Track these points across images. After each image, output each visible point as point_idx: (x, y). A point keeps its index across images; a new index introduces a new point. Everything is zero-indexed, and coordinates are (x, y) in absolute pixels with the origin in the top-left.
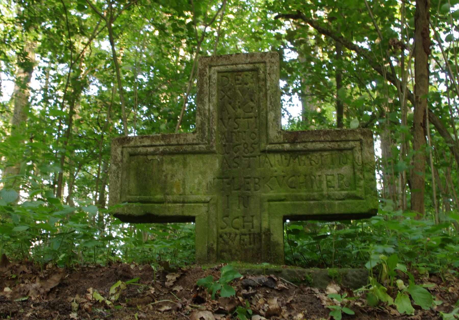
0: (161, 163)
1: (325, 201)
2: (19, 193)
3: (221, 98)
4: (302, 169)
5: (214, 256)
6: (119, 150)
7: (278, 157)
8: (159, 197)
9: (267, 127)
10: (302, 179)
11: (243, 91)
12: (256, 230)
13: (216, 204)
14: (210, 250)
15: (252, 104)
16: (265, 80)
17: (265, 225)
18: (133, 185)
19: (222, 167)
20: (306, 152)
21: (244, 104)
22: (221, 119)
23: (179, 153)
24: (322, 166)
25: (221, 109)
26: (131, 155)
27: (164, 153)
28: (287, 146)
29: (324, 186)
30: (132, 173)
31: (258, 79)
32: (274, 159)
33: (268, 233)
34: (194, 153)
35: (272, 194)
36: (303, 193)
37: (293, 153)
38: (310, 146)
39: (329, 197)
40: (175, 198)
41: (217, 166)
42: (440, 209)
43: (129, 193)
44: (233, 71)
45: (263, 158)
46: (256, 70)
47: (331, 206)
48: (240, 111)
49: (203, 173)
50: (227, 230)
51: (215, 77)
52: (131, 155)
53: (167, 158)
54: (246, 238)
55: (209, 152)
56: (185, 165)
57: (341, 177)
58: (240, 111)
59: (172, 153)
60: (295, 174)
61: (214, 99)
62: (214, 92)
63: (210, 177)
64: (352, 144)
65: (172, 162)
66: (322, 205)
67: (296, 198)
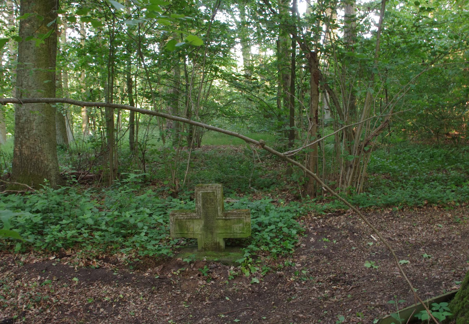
0: (186, 222)
1: (235, 234)
2: (205, 6)
3: (203, 201)
4: (228, 224)
5: (203, 249)
6: (172, 218)
7: (221, 220)
8: (186, 232)
9: (217, 212)
10: (228, 227)
11: (210, 199)
12: (215, 242)
13: (203, 235)
14: (202, 248)
15: (213, 203)
16: (217, 196)
17: (218, 241)
18: (178, 228)
19: (204, 223)
20: (230, 219)
21: (210, 203)
22: (203, 208)
23: (191, 219)
24: (234, 223)
25: (203, 205)
26: (176, 219)
27: (186, 219)
28: (224, 218)
29: (235, 229)
30: (177, 225)
31: (215, 196)
32: (220, 221)
33: (219, 243)
34: (196, 219)
35: (219, 232)
36: (229, 231)
37: (226, 220)
38: (231, 218)
39: (236, 233)
40: (191, 233)
41: (203, 223)
42: (270, 5)
43: (177, 231)
44: (206, 193)
45: (217, 221)
46: (214, 193)
47: (237, 235)
48: (209, 206)
49: (199, 225)
50: (207, 242)
51: (201, 194)
52: (176, 219)
53: (188, 220)
54: (213, 244)
55: (200, 219)
56: (193, 222)
57: (240, 227)
58: (209, 206)
59: (189, 219)
60: (226, 226)
61: (201, 202)
62: (201, 200)
63: (201, 226)
64: (243, 217)
65: (189, 221)
66: (234, 236)
67: (227, 233)
